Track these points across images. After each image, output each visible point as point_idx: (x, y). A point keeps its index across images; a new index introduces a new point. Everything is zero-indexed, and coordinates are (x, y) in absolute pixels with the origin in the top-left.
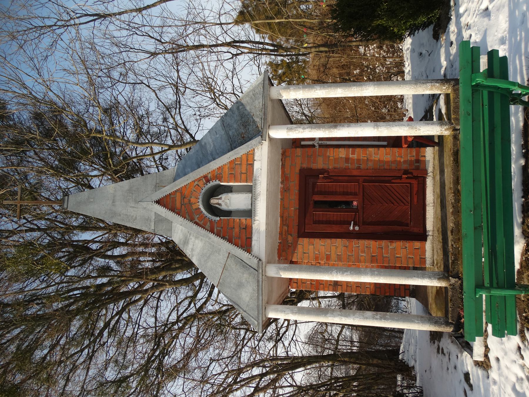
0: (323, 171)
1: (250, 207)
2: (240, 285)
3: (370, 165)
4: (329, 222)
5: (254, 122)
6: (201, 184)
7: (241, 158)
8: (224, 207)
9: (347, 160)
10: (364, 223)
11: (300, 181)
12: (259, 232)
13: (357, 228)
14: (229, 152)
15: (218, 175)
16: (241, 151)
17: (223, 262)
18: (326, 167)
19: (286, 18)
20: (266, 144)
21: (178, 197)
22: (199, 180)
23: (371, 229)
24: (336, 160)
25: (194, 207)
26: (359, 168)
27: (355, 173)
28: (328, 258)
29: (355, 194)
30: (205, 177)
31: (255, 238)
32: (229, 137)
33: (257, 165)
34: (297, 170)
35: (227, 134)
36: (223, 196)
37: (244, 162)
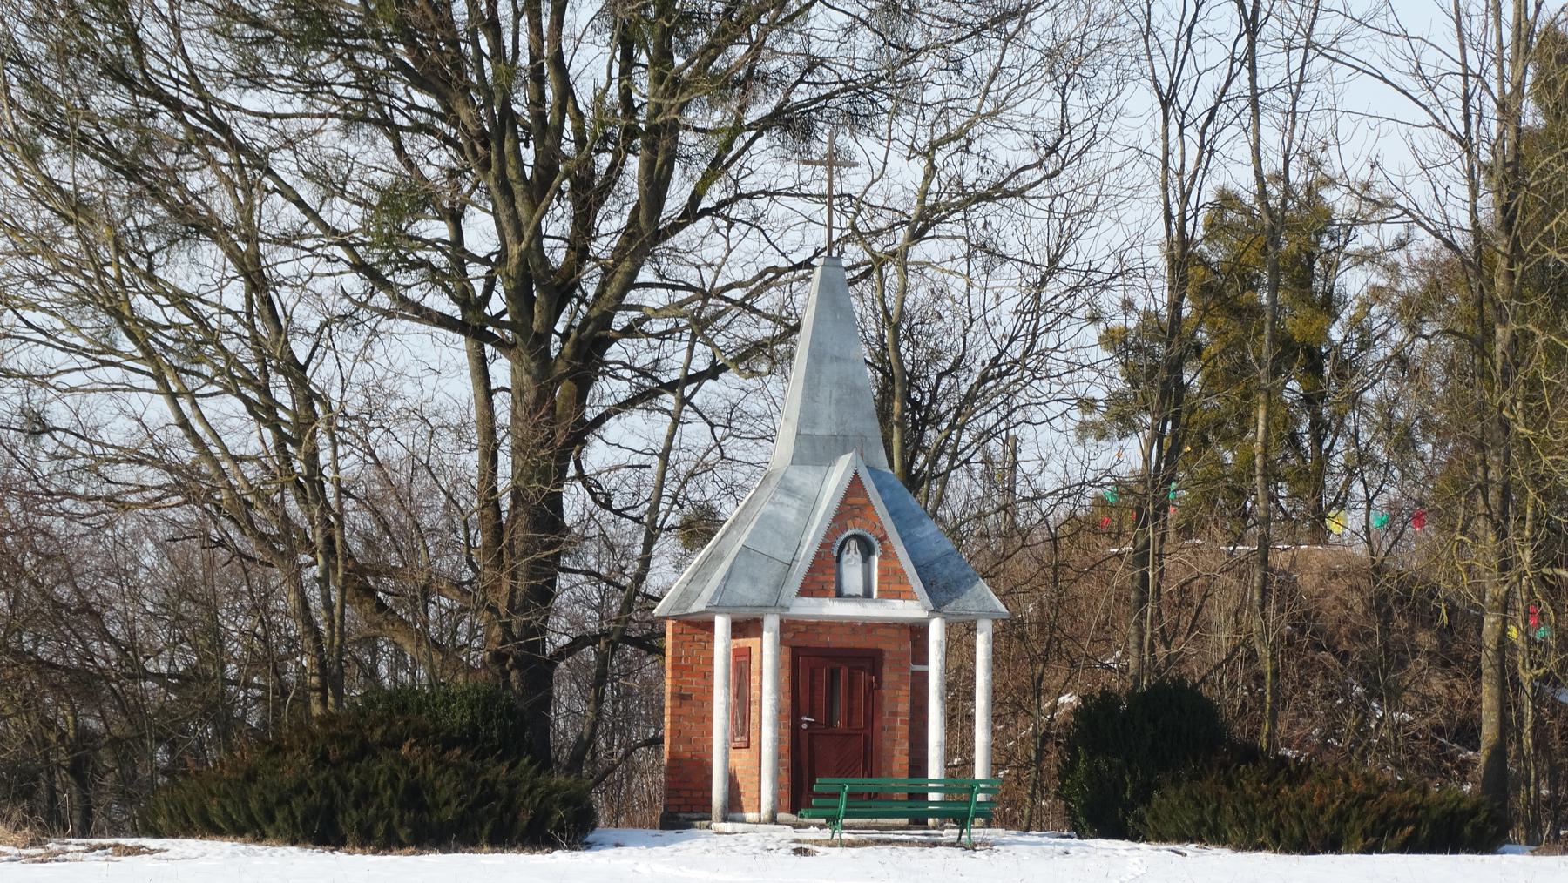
0: (879, 682)
1: (846, 592)
2: (754, 581)
3: (887, 744)
4: (812, 689)
5: (951, 600)
6: (877, 531)
7: (907, 583)
8: (845, 557)
9: (895, 714)
10: (812, 736)
11: (854, 649)
12: (821, 605)
13: (805, 726)
14: (914, 563)
15: (888, 554)
16: (916, 585)
17: (776, 555)
18: (885, 685)
19: (1551, 231)
20: (924, 615)
21: (860, 500)
22: (882, 529)
23: (805, 743)
24: (895, 700)
25: (849, 523)
26: (883, 729)
27: (876, 724)
28: (1470, 702)
29: (849, 723)
30: (885, 537)
31: (813, 600)
32: (932, 563)
33: (898, 603)
34: (881, 646)
35: (937, 560)
36: (859, 557)
37: (902, 588)
